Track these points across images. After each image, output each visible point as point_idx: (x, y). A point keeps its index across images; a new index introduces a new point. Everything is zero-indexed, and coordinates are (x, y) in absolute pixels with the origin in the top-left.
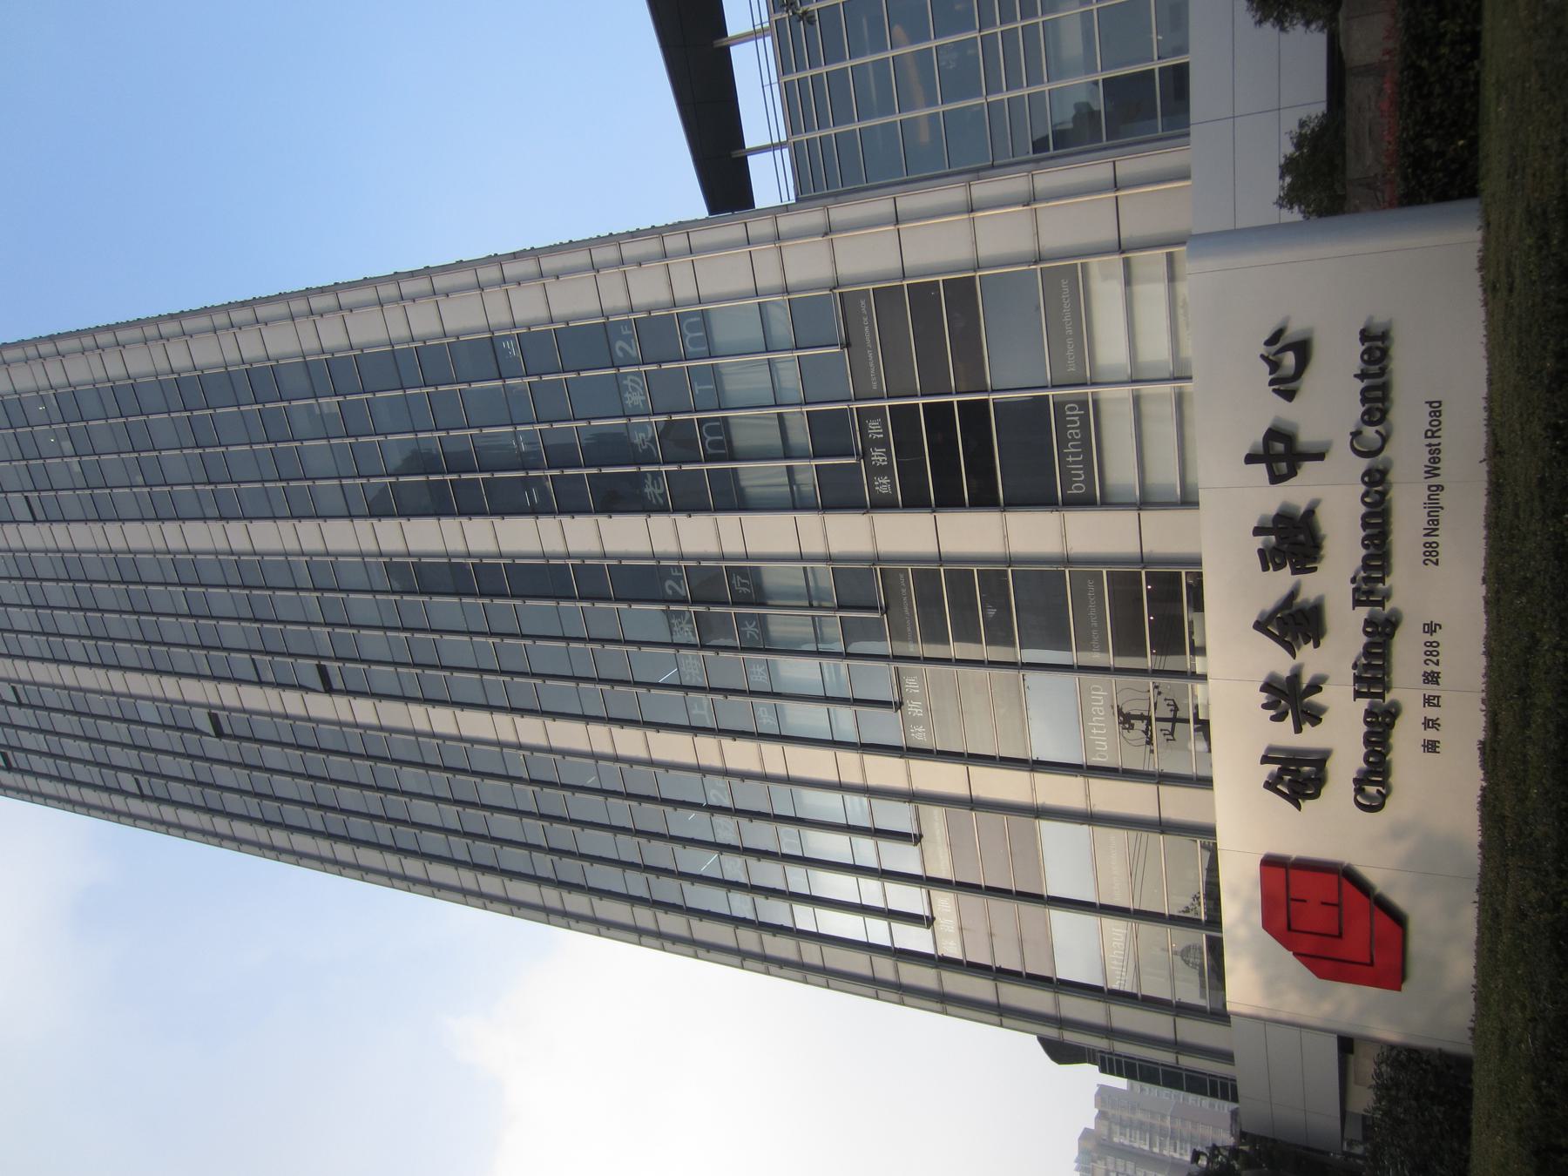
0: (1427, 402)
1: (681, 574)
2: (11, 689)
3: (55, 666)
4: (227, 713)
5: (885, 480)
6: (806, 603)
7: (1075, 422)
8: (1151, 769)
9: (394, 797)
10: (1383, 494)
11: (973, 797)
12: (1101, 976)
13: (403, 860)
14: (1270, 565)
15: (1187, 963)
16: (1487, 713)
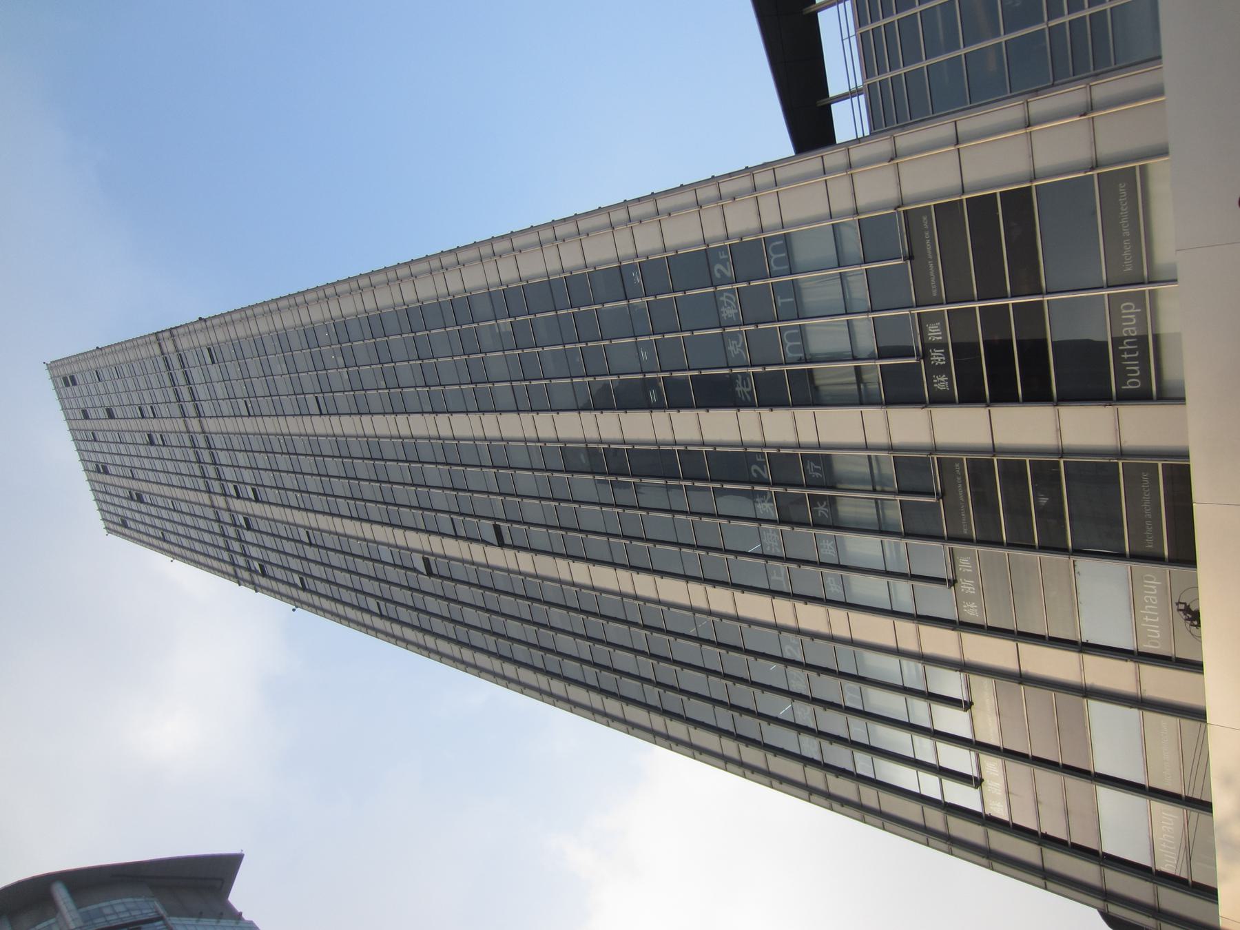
1: (764, 460)
2: (306, 533)
3: (390, 529)
4: (475, 567)
5: (943, 378)
6: (870, 488)
7: (1131, 320)
9: (601, 647)
11: (1022, 672)
12: (1149, 857)
13: (604, 699)
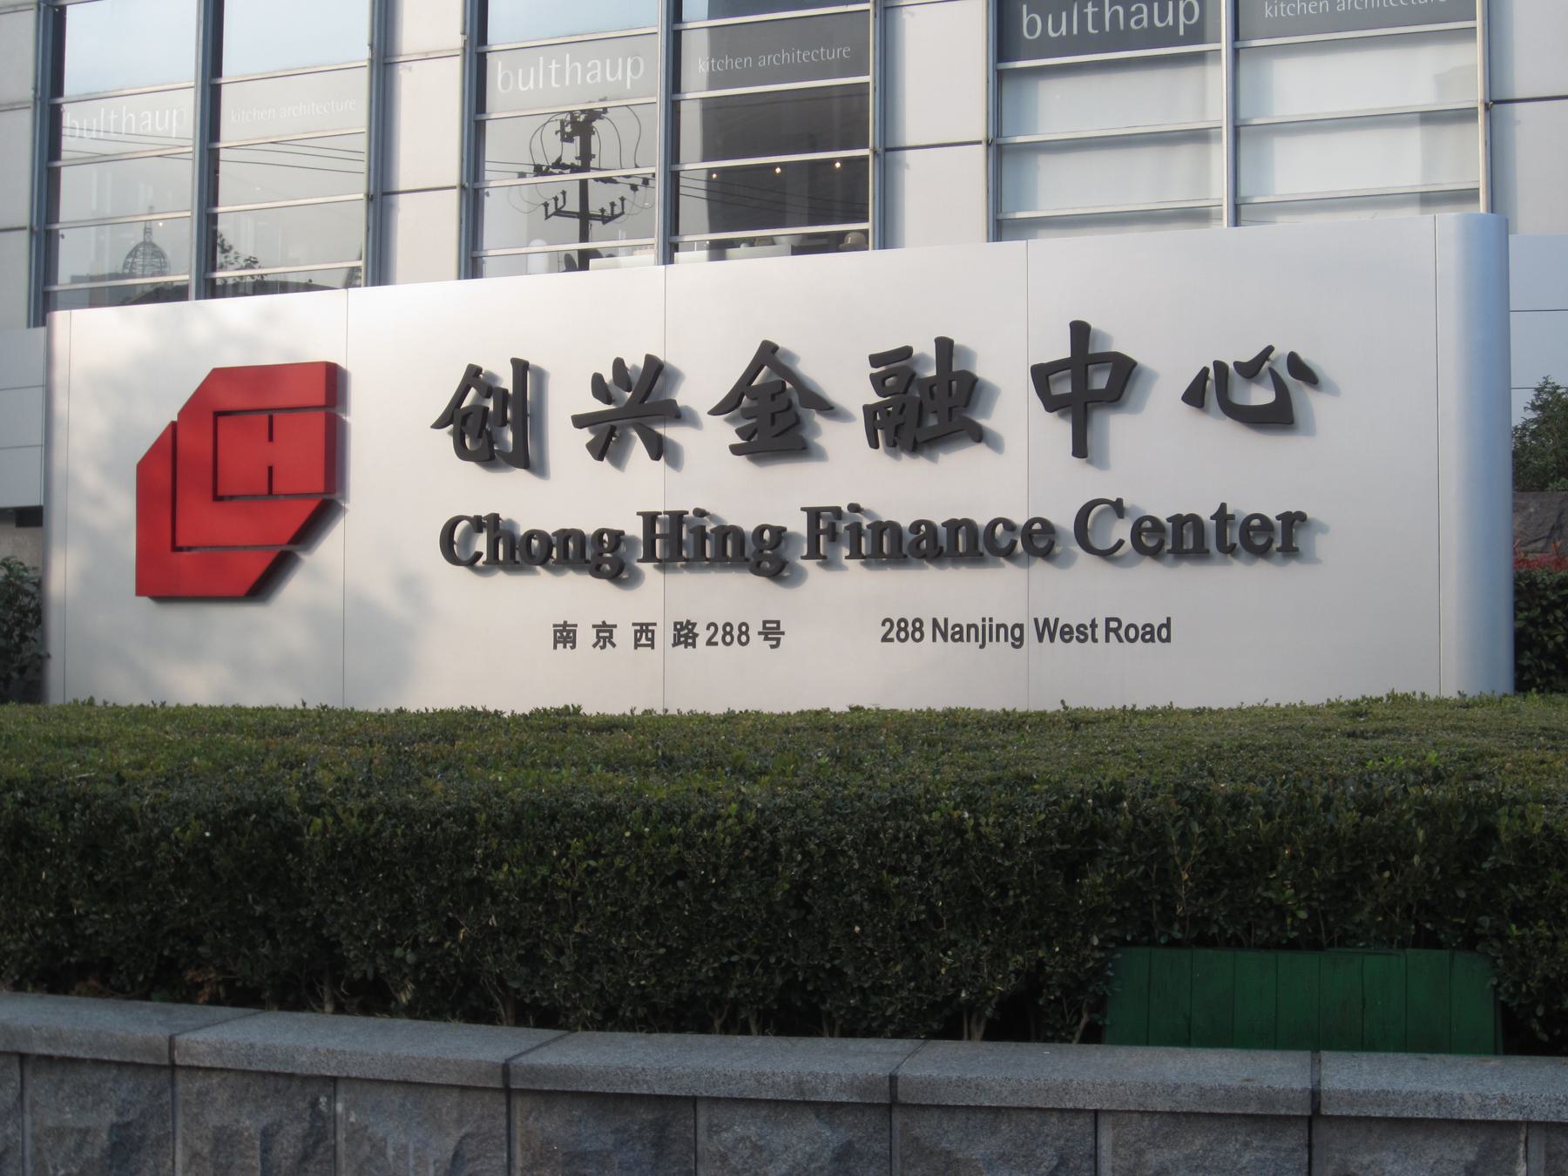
0: (1169, 619)
8: (488, 175)
10: (1009, 553)
14: (882, 369)
15: (133, 253)
16: (629, 718)
